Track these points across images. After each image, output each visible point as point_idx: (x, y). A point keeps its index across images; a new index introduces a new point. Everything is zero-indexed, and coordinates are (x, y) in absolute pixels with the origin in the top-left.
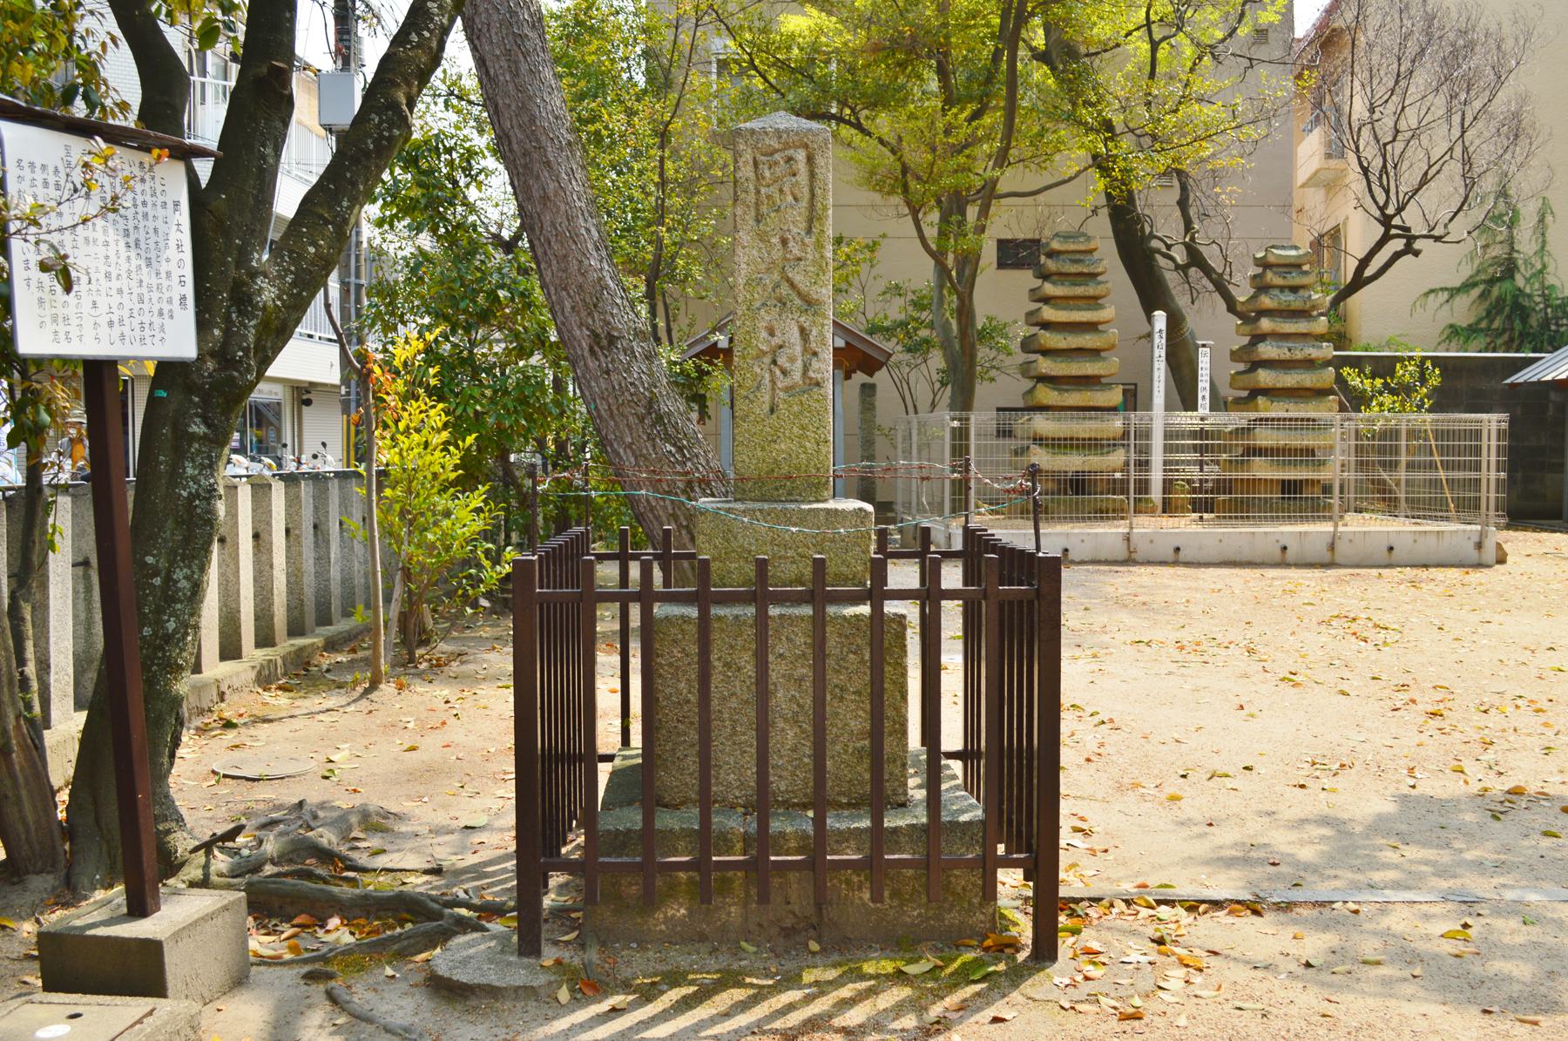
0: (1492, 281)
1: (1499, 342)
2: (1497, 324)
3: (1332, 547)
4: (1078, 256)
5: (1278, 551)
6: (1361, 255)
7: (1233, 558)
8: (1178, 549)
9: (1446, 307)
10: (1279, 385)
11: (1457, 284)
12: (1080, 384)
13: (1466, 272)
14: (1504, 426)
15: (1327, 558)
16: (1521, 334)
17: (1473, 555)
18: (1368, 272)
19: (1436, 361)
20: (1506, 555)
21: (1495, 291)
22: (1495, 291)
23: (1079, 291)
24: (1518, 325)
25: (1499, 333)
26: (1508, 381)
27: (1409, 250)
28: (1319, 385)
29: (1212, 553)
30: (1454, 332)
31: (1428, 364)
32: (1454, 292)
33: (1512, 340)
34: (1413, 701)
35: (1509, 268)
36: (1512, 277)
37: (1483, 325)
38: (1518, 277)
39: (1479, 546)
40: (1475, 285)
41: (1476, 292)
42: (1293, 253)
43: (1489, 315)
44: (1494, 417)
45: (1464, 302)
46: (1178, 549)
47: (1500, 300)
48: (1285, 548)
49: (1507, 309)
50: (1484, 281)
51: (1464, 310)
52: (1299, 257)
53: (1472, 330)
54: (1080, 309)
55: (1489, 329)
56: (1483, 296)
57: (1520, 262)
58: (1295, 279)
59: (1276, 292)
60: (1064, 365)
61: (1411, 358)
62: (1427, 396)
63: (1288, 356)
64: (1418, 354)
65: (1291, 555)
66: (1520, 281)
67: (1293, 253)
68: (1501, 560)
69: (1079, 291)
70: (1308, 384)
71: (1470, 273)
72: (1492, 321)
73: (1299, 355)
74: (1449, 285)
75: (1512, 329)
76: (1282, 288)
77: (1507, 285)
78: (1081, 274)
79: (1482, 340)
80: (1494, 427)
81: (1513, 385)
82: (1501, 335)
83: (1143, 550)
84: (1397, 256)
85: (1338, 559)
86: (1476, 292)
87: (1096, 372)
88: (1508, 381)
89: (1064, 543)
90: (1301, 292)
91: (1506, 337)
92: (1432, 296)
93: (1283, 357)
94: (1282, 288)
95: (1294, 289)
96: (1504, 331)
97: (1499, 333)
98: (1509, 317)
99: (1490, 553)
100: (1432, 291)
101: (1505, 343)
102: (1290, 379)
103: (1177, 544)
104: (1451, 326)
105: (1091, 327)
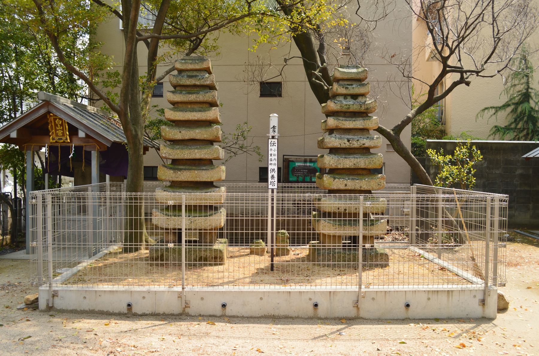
0: (517, 104)
1: (521, 135)
2: (520, 126)
3: (356, 305)
4: (195, 73)
5: (311, 307)
6: (431, 83)
7: (272, 313)
8: (224, 306)
9: (494, 117)
10: (340, 166)
11: (500, 104)
12: (194, 165)
13: (504, 99)
14: (505, 204)
15: (353, 313)
16: (532, 131)
17: (478, 310)
18: (439, 92)
19: (480, 146)
20: (507, 304)
21: (519, 110)
22: (519, 110)
23: (192, 97)
24: (531, 126)
25: (521, 130)
26: (525, 156)
27: (462, 81)
28: (370, 166)
29: (254, 308)
30: (497, 130)
31: (474, 148)
32: (498, 109)
33: (528, 134)
34: (464, 346)
35: (526, 96)
36: (528, 102)
37: (513, 126)
38: (531, 101)
39: (483, 302)
40: (509, 105)
41: (509, 109)
42: (354, 70)
43: (516, 121)
44: (497, 196)
45: (503, 114)
46: (224, 306)
47: (523, 113)
48: (316, 305)
49: (525, 118)
50: (513, 104)
51: (503, 118)
52: (358, 73)
53: (507, 129)
54: (193, 110)
55: (516, 128)
56: (514, 111)
57: (532, 95)
58: (355, 89)
59: (341, 98)
60: (178, 151)
61: (464, 144)
62: (473, 166)
63: (347, 145)
64: (469, 141)
65: (322, 311)
66: (532, 104)
67: (354, 70)
68: (503, 308)
69: (192, 97)
70: (362, 166)
71: (507, 101)
72: (517, 125)
73: (356, 145)
74: (495, 105)
75: (528, 129)
76: (345, 96)
77: (525, 105)
78: (195, 86)
79: (512, 134)
80: (497, 205)
81: (527, 159)
82: (522, 131)
83: (195, 307)
84: (455, 84)
85: (362, 314)
86: (509, 109)
87: (207, 157)
88: (525, 156)
89: (127, 299)
90: (360, 99)
91: (525, 132)
92: (486, 111)
93: (343, 146)
94: (345, 96)
95: (355, 97)
96: (524, 129)
97: (521, 130)
98: (527, 122)
99: (492, 303)
100: (486, 109)
101: (524, 136)
102: (348, 162)
103: (223, 301)
104: (496, 127)
105: (209, 123)
